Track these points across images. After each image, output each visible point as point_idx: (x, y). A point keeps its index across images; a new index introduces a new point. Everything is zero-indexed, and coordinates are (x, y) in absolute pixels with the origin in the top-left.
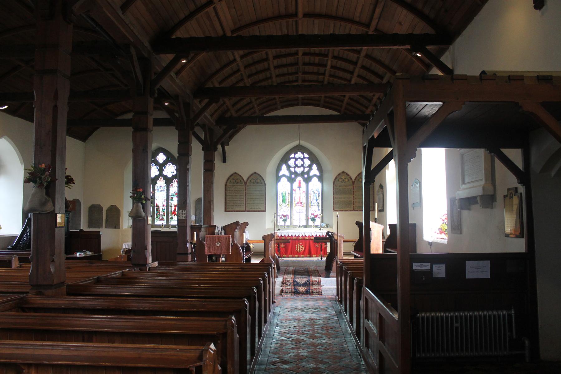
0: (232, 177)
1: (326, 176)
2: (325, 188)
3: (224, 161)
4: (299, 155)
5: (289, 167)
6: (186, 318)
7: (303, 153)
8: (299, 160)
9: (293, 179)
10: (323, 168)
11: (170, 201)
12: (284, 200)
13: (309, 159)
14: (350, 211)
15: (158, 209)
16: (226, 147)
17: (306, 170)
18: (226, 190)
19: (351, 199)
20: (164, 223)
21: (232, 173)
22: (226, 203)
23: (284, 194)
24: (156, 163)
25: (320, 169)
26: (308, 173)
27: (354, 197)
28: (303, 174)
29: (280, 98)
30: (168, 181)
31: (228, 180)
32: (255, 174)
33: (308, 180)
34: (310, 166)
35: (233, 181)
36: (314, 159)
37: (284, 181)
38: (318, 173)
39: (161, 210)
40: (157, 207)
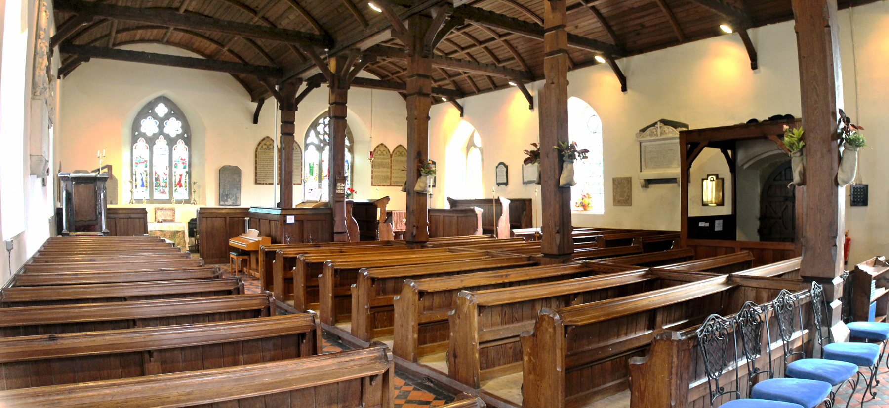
0: (264, 142)
5: (318, 133)
6: (100, 332)
10: (355, 139)
11: (174, 169)
12: (311, 172)
14: (388, 186)
15: (157, 179)
18: (256, 157)
19: (389, 174)
20: (166, 197)
22: (256, 173)
23: (312, 165)
24: (155, 117)
30: (171, 142)
31: (258, 145)
32: (400, 147)
35: (265, 147)
37: (312, 148)
39: (161, 179)
40: (156, 176)
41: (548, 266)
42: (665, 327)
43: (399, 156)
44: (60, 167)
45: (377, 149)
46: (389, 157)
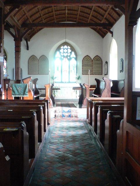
1: (78, 58)
2: (78, 64)
3: (28, 49)
4: (66, 47)
5: (60, 53)
7: (67, 46)
8: (66, 50)
9: (62, 59)
13: (70, 49)
14: (100, 75)
16: (28, 42)
17: (69, 54)
21: (32, 55)
25: (76, 54)
26: (70, 56)
27: (92, 68)
28: (67, 56)
29: (55, 6)
31: (29, 59)
33: (70, 59)
34: (71, 53)
36: (73, 49)
38: (75, 57)
41: (6, 118)
42: (126, 178)
43: (96, 61)
44: (62, 68)
45: (85, 58)
46: (91, 61)
